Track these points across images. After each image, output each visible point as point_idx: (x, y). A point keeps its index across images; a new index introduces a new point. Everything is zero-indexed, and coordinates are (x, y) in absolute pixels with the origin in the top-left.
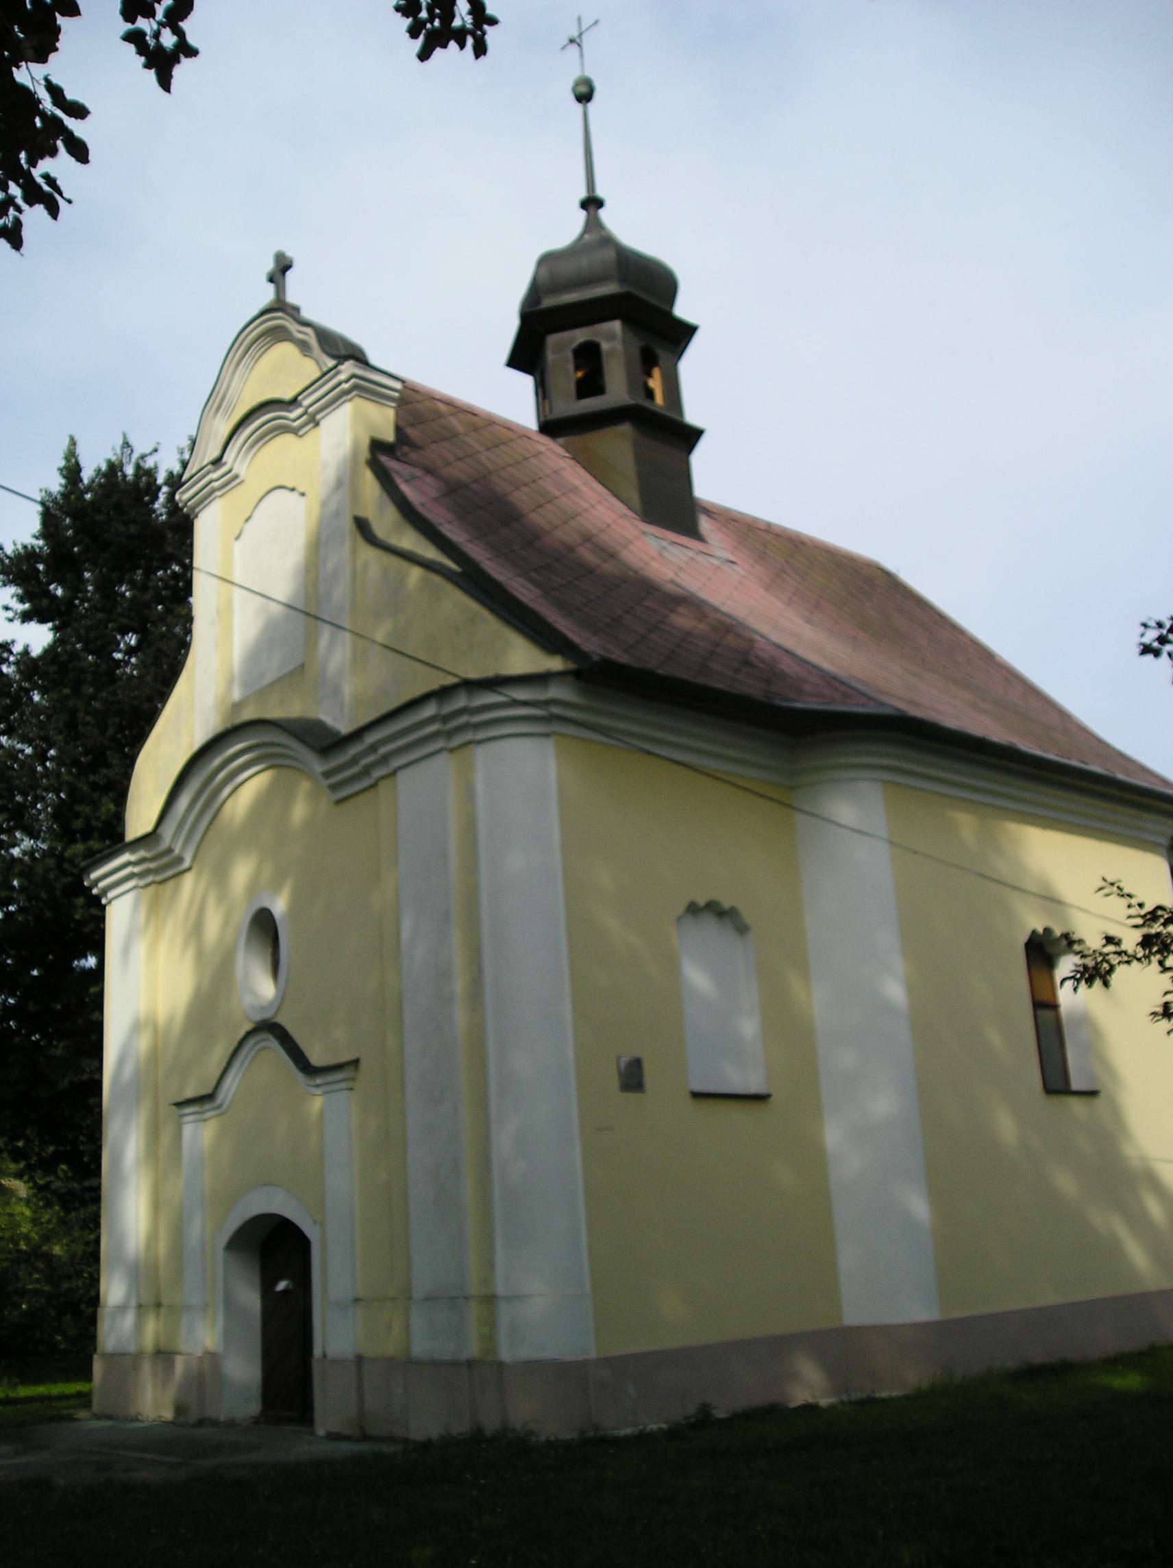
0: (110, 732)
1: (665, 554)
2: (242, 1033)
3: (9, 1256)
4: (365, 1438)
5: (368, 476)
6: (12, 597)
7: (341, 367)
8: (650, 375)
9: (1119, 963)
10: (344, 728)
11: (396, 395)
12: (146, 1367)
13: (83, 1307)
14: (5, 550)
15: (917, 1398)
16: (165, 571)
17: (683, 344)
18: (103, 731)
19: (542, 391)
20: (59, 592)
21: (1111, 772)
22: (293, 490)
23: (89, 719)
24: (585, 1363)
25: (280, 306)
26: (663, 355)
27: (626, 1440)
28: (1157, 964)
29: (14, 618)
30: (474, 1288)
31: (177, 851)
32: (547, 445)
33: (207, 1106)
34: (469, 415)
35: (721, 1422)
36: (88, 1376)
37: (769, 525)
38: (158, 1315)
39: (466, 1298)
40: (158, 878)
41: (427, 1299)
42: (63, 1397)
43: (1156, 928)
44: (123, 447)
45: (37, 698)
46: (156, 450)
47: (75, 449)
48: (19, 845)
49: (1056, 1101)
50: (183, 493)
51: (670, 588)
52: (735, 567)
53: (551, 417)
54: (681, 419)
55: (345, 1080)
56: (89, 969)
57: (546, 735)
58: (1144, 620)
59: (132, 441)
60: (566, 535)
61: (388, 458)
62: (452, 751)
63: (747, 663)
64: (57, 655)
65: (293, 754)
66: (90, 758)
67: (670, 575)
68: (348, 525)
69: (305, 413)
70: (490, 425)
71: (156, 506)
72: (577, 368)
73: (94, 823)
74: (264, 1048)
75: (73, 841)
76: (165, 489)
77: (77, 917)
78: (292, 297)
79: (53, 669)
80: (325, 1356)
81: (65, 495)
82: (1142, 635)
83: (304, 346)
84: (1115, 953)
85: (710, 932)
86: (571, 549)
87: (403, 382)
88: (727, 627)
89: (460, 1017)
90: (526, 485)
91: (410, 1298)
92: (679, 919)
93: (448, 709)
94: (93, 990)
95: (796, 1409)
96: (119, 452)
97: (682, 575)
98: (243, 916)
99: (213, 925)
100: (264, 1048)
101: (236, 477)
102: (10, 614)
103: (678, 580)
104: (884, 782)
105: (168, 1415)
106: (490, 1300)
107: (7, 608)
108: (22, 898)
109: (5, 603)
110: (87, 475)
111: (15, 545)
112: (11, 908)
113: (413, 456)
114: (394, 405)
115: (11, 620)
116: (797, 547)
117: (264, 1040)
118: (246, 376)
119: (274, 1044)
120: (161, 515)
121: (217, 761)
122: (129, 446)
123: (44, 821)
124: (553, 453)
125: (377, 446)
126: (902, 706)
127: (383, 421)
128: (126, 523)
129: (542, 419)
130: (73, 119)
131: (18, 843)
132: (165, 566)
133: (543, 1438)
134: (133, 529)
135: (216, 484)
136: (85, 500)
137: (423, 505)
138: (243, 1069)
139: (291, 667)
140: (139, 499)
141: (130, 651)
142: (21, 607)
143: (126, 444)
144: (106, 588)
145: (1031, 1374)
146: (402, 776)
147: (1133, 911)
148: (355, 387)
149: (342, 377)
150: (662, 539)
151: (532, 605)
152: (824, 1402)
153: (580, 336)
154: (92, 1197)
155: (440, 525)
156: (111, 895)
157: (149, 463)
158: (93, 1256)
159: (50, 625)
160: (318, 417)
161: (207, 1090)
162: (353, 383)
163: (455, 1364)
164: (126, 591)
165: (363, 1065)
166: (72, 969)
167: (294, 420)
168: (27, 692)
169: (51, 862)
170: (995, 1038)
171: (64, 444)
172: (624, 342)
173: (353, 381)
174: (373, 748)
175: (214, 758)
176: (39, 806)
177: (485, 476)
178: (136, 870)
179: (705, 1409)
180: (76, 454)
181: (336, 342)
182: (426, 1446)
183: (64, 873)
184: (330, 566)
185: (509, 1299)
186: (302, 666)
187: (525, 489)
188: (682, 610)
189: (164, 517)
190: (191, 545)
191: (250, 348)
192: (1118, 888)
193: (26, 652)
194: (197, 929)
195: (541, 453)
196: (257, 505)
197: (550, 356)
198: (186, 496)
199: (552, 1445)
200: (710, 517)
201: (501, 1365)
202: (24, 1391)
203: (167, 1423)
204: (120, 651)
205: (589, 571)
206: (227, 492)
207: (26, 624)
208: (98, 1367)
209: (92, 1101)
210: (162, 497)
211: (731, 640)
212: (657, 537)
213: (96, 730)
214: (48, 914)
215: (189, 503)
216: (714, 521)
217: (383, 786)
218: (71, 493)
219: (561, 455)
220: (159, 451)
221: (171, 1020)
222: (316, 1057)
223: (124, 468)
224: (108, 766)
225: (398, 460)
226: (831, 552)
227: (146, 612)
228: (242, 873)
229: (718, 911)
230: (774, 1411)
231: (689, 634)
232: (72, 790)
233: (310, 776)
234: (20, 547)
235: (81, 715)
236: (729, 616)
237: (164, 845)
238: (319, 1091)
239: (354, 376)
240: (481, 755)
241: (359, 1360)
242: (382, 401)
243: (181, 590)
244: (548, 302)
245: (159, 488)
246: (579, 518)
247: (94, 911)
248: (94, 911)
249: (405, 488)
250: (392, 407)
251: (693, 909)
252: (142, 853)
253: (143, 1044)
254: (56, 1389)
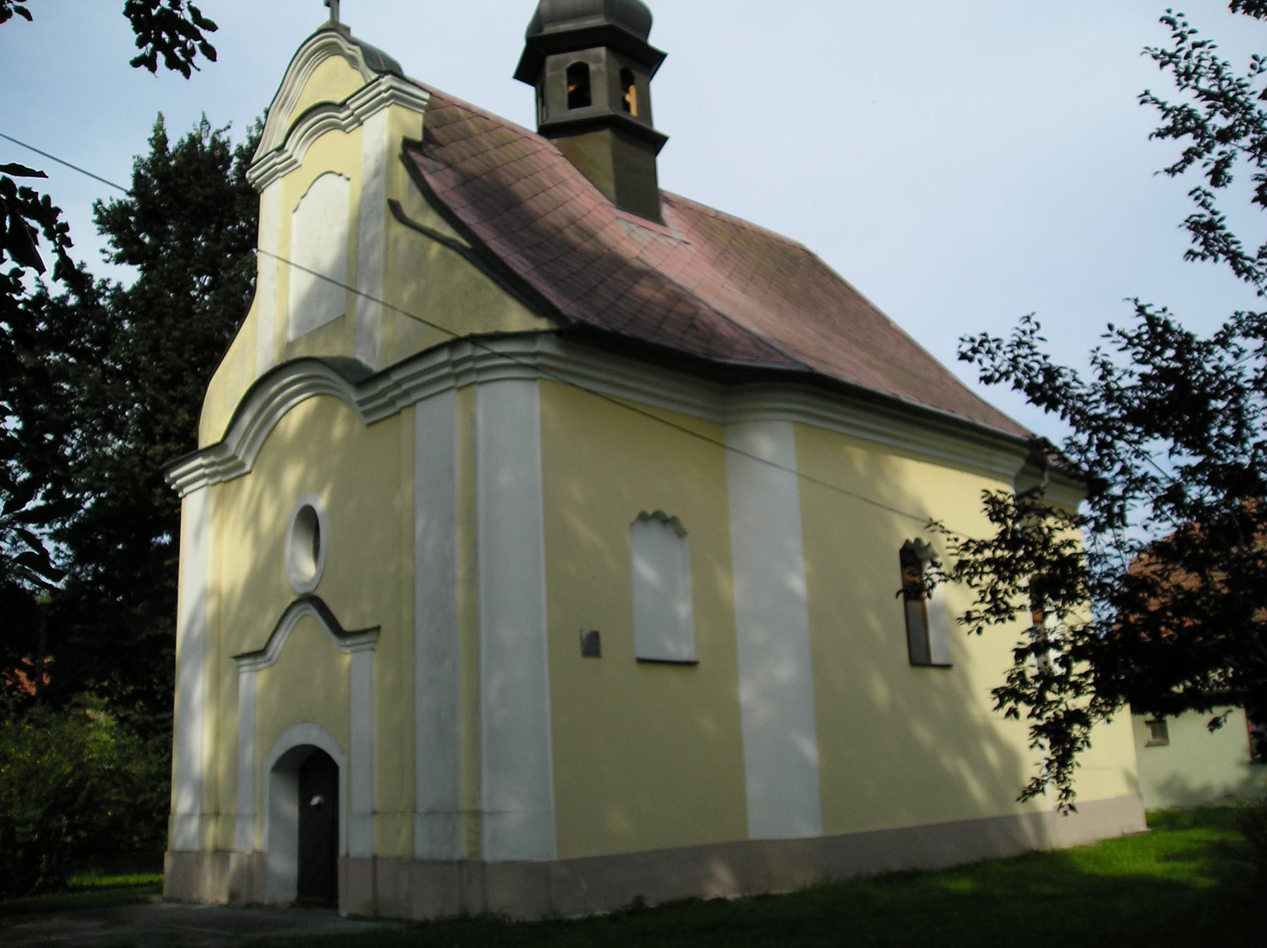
0: (187, 356)
1: (634, 235)
2: (289, 603)
3: (98, 773)
4: (377, 918)
5: (400, 168)
6: (109, 243)
7: (381, 80)
8: (627, 91)
9: (939, 581)
10: (376, 367)
11: (425, 103)
12: (207, 862)
13: (154, 814)
14: (104, 204)
15: (802, 896)
16: (234, 226)
17: (655, 67)
18: (181, 355)
19: (541, 98)
20: (147, 240)
21: (972, 419)
22: (340, 175)
23: (169, 345)
24: (547, 865)
25: (334, 26)
26: (638, 75)
27: (579, 923)
28: (966, 582)
29: (109, 260)
30: (465, 805)
31: (240, 458)
32: (543, 145)
33: (260, 660)
34: (483, 119)
35: (651, 911)
36: (158, 866)
37: (717, 212)
38: (217, 820)
39: (458, 813)
41: (430, 812)
42: (138, 885)
43: (968, 556)
44: (202, 124)
45: (126, 325)
46: (229, 127)
47: (162, 124)
48: (110, 446)
49: (918, 670)
50: (251, 172)
51: (636, 263)
52: (689, 247)
53: (549, 121)
54: (650, 128)
55: (369, 642)
56: (163, 544)
57: (534, 380)
58: (961, 336)
59: (209, 120)
60: (555, 219)
61: (417, 154)
62: (459, 389)
63: (693, 326)
64: (145, 292)
65: (336, 386)
66: (169, 376)
67: (636, 252)
69: (352, 114)
70: (499, 127)
71: (228, 173)
72: (570, 83)
73: (172, 429)
74: (305, 616)
75: (154, 443)
76: (236, 160)
77: (156, 504)
78: (344, 20)
79: (141, 303)
80: (348, 855)
81: (154, 161)
82: (960, 347)
83: (352, 61)
84: (938, 573)
85: (655, 535)
86: (559, 231)
87: (431, 94)
88: (679, 297)
89: (460, 595)
90: (526, 177)
91: (415, 812)
92: (632, 524)
93: (457, 356)
94: (168, 563)
95: (710, 902)
96: (198, 127)
97: (646, 252)
98: (292, 510)
99: (268, 516)
100: (305, 616)
101: (295, 162)
102: (107, 257)
103: (641, 256)
104: (796, 422)
105: (224, 899)
106: (477, 814)
107: (103, 251)
108: (112, 489)
109: (102, 247)
110: (172, 145)
111: (112, 200)
112: (103, 495)
113: (437, 152)
114: (422, 111)
115: (107, 262)
116: (738, 230)
117: (305, 609)
118: (306, 80)
119: (313, 612)
120: (232, 181)
121: (275, 388)
122: (207, 124)
123: (131, 426)
124: (548, 148)
125: (408, 144)
126: (812, 363)
127: (413, 123)
128: (203, 187)
129: (540, 124)
130: (206, 31)
131: (109, 443)
132: (234, 221)
133: (514, 920)
134: (209, 191)
135: (279, 167)
136: (170, 166)
137: (443, 193)
138: (288, 633)
139: (336, 316)
140: (214, 166)
141: (204, 290)
142: (115, 251)
143: (205, 122)
144: (186, 237)
145: (890, 878)
146: (419, 406)
147: (951, 543)
148: (392, 96)
149: (383, 88)
150: (631, 223)
151: (525, 277)
152: (731, 896)
153: (573, 58)
154: (166, 727)
155: (456, 209)
156: (186, 490)
157: (223, 138)
158: (164, 775)
159: (139, 266)
160: (362, 118)
161: (260, 647)
162: (391, 93)
163: (448, 863)
164: (202, 241)
165: (383, 631)
166: (151, 544)
167: (343, 120)
168: (120, 320)
169: (136, 459)
170: (874, 622)
171: (154, 120)
172: (608, 64)
173: (391, 91)
174: (398, 384)
176: (127, 413)
177: (493, 170)
178: (207, 471)
179: (639, 900)
180: (164, 128)
181: (377, 59)
182: (424, 925)
183: (147, 469)
184: (368, 237)
185: (491, 814)
186: (344, 316)
187: (524, 181)
188: (642, 281)
189: (234, 183)
190: (258, 206)
191: (309, 59)
192: (941, 526)
193: (119, 288)
194: (255, 518)
195: (538, 151)
196: (311, 186)
197: (549, 73)
198: (254, 175)
199: (522, 925)
200: (670, 205)
201: (484, 864)
202: (107, 881)
203: (222, 906)
204: (196, 290)
205: (573, 248)
206: (287, 174)
207: (119, 265)
208: (168, 862)
209: (165, 651)
210: (233, 167)
211: (681, 307)
212: (627, 221)
213: (174, 354)
214: (133, 501)
215: (257, 181)
216: (673, 209)
217: (404, 413)
218: (159, 160)
219: (553, 153)
220: (232, 128)
221: (232, 591)
222: (347, 623)
223: (203, 142)
224: (184, 383)
225: (423, 154)
226: (766, 236)
227: (218, 260)
228: (292, 475)
229: (662, 519)
230: (692, 903)
231: (648, 301)
232: (154, 403)
233: (347, 403)
234: (116, 202)
235: (163, 341)
236: (680, 287)
237: (229, 453)
238: (348, 650)
239: (391, 87)
240: (482, 392)
241: (375, 858)
242: (416, 109)
243: (250, 239)
244: (549, 30)
245: (231, 159)
246: (566, 205)
247: (170, 499)
248: (170, 499)
249: (430, 179)
250: (420, 113)
251: (643, 517)
252: (212, 459)
253: (210, 608)
254: (133, 879)
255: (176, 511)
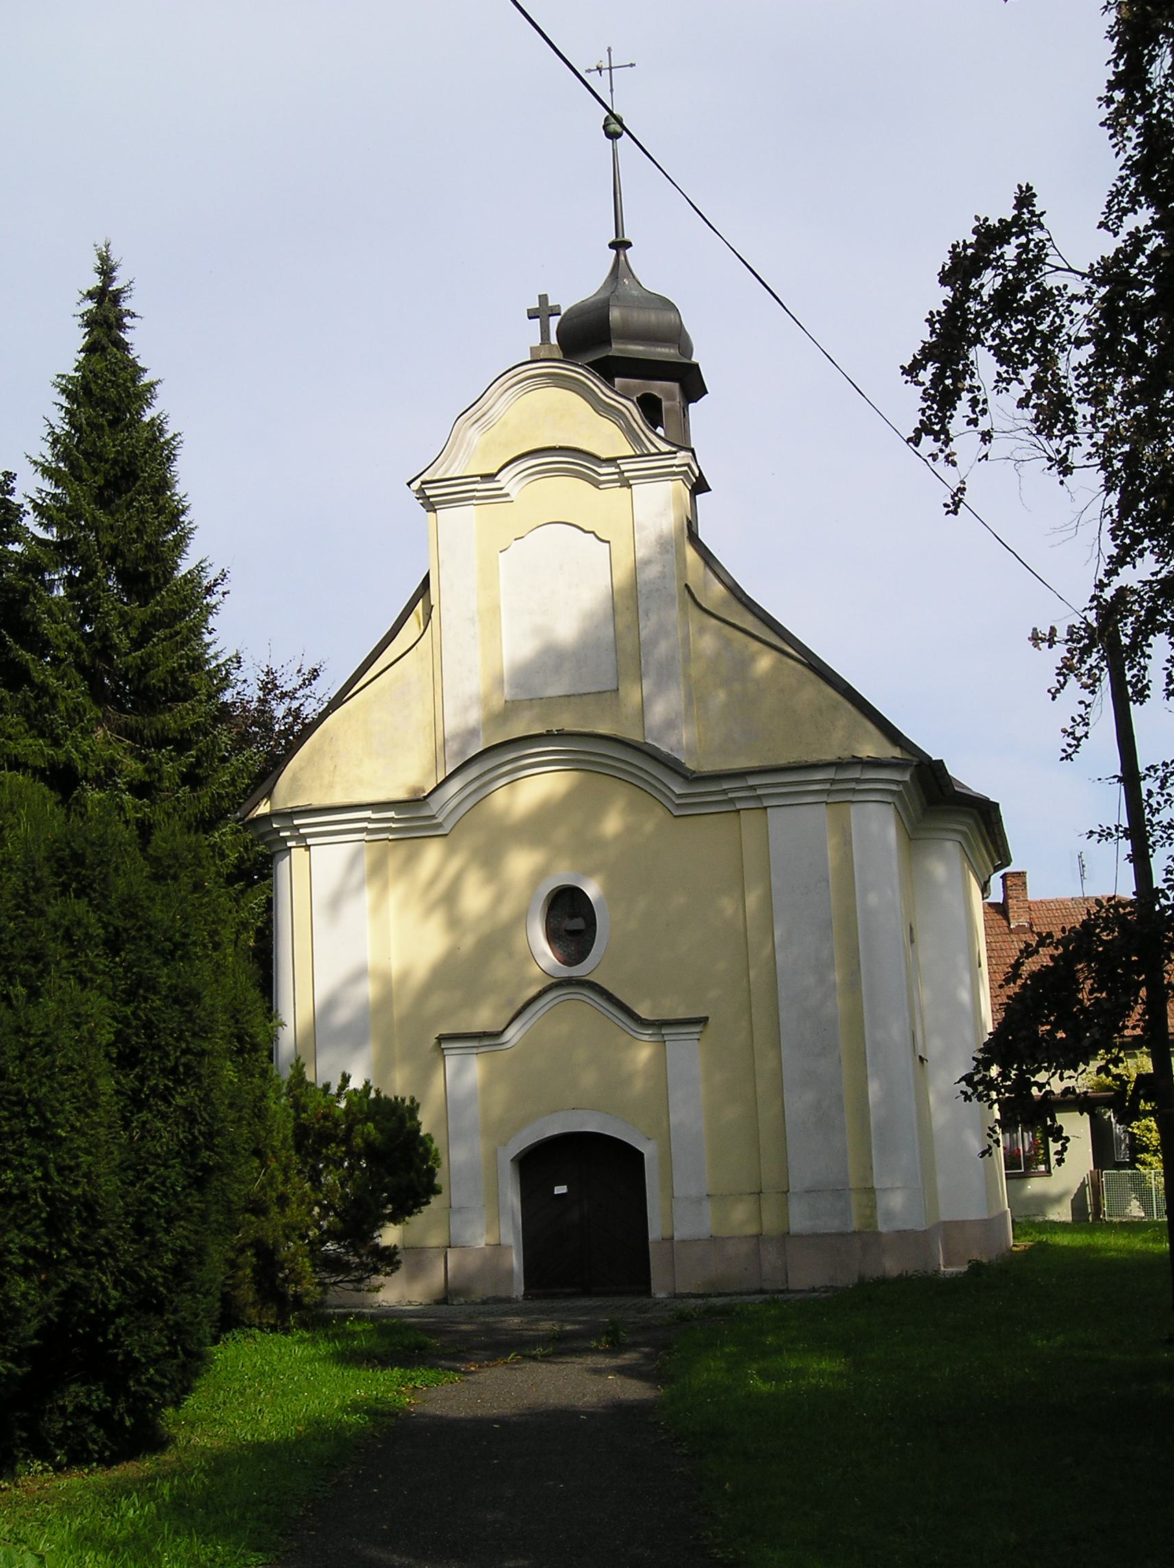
30: (853, 1183)
40: (368, 838)
68: (675, 587)
101: (507, 495)
106: (871, 1191)
149: (676, 462)
163: (842, 1235)
173: (686, 468)
175: (509, 752)
255: (255, 901)
